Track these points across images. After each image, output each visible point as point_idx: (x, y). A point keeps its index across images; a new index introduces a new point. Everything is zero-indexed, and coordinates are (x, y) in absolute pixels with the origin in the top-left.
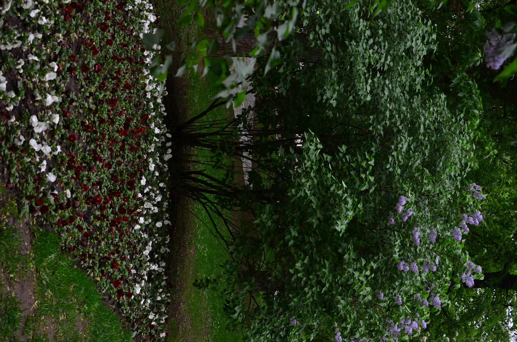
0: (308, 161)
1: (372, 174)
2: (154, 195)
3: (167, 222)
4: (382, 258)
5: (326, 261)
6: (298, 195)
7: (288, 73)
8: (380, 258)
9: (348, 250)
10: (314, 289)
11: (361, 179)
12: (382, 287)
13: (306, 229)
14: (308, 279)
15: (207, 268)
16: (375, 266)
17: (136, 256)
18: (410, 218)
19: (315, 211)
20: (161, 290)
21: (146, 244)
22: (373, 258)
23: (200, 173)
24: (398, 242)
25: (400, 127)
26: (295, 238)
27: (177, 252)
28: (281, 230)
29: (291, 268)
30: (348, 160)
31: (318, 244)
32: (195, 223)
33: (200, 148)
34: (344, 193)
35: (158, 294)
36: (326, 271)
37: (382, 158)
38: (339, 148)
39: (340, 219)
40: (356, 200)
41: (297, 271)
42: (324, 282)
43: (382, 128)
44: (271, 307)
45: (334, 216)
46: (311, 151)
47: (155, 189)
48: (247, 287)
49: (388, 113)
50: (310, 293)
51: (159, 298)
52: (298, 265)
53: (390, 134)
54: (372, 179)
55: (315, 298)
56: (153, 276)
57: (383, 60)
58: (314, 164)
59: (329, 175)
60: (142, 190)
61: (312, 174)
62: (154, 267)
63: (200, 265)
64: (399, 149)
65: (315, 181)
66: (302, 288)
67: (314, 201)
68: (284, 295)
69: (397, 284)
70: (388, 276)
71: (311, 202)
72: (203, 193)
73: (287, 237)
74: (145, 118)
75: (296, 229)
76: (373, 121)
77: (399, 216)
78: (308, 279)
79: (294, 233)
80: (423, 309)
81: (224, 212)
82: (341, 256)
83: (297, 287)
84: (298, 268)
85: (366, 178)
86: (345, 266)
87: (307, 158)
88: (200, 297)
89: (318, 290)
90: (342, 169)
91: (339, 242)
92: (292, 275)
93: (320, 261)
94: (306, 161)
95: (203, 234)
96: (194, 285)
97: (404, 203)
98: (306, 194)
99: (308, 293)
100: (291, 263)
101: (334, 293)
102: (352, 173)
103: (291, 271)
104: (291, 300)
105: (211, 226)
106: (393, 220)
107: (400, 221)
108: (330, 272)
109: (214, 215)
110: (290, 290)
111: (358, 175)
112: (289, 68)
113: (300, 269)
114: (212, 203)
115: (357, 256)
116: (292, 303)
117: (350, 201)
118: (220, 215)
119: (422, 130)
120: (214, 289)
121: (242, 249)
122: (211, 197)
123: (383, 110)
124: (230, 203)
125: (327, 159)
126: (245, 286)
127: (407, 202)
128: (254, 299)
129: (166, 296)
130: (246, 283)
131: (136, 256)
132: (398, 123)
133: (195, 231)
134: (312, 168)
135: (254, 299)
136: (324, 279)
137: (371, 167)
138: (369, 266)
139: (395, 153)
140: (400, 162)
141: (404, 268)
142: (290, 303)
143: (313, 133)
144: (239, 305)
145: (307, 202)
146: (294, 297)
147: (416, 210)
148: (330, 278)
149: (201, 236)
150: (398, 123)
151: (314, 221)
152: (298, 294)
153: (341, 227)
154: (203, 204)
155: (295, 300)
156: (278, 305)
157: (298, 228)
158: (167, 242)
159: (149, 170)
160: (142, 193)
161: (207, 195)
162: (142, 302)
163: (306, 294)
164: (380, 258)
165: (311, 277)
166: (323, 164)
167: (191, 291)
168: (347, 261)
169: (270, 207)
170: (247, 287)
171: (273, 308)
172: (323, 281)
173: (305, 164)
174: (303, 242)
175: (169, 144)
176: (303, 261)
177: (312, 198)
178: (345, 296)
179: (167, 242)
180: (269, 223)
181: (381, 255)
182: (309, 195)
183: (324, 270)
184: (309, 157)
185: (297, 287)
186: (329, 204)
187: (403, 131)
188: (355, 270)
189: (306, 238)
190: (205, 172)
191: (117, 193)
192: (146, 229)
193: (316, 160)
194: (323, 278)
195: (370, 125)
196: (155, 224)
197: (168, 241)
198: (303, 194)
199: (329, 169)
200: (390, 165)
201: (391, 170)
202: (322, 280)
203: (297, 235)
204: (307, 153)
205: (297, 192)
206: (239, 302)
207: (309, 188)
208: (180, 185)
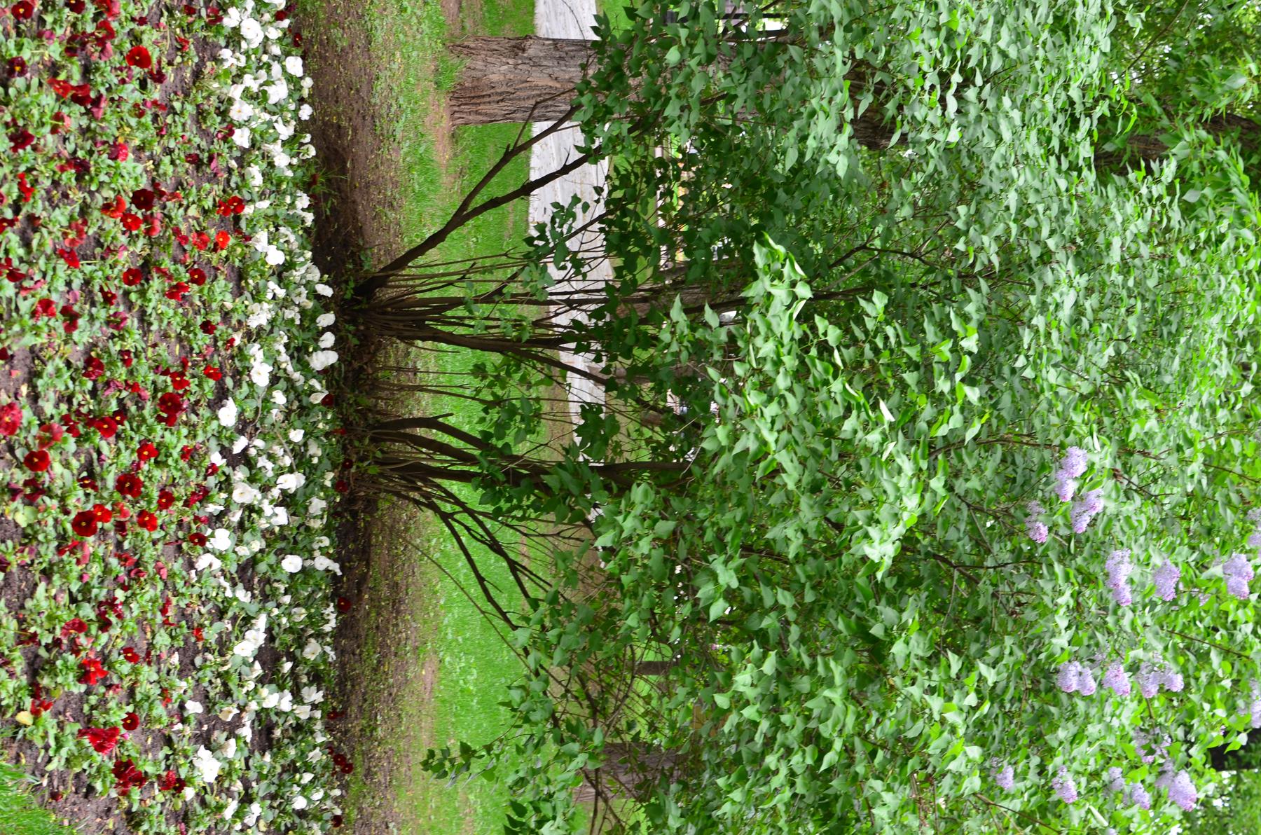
0: (766, 340)
1: (969, 380)
2: (269, 465)
3: (322, 563)
4: (1011, 654)
5: (832, 664)
6: (738, 448)
7: (693, 63)
8: (1007, 651)
9: (903, 628)
10: (796, 759)
11: (938, 400)
12: (1009, 747)
13: (760, 555)
14: (777, 725)
15: (479, 726)
16: (991, 676)
17: (205, 660)
18: (1093, 524)
19: (791, 502)
20: (308, 777)
21: (247, 621)
22: (982, 654)
23: (432, 423)
24: (1065, 599)
25: (1051, 243)
26: (730, 595)
27: (375, 670)
28: (682, 564)
29: (721, 690)
30: (893, 340)
31: (807, 613)
32: (435, 593)
33: (429, 344)
34: (885, 438)
35: (296, 789)
36: (836, 695)
37: (1004, 328)
38: (862, 303)
39: (878, 522)
40: (924, 465)
41: (740, 702)
42: (825, 735)
43: (994, 248)
44: (659, 822)
45: (860, 515)
46: (777, 307)
47: (278, 451)
48: (581, 759)
49: (1012, 199)
50: (784, 771)
51: (300, 803)
52: (743, 680)
53: (1015, 270)
54: (973, 394)
55: (800, 789)
56: (278, 733)
57: (986, 36)
58: (784, 351)
59: (837, 386)
60: (226, 444)
61: (782, 382)
62: (274, 699)
63: (455, 715)
64: (1052, 308)
65: (793, 403)
66: (758, 759)
67: (787, 465)
68: (699, 784)
69: (1062, 734)
70: (1032, 711)
71: (779, 470)
72: (408, 431)
73: (705, 591)
74: (231, 207)
75: (732, 565)
76: (968, 224)
77: (1064, 516)
78: (777, 725)
79: (728, 578)
80: (1130, 819)
81: (505, 536)
82: (877, 650)
83: (739, 754)
84: (741, 689)
85: (953, 391)
86: (897, 681)
87: (762, 329)
88: (456, 810)
89: (809, 761)
90: (874, 367)
91: (872, 604)
92: (724, 714)
93: (814, 666)
94: (759, 341)
95: (461, 624)
96: (426, 765)
97: (1081, 468)
98: (765, 443)
99: (776, 772)
100: (719, 675)
101: (860, 769)
102: (910, 378)
103: (722, 701)
104: (720, 795)
105: (476, 590)
106: (1044, 530)
107: (1064, 531)
108: (850, 696)
109: (480, 553)
110: (719, 765)
111: (927, 384)
112: (696, 51)
113: (751, 693)
114: (471, 513)
115: (930, 647)
116: (727, 808)
117: (908, 467)
118: (496, 547)
119: (1115, 256)
120: (489, 774)
121: (560, 636)
122: (466, 492)
123: (997, 187)
124: (520, 501)
125: (825, 334)
126: (573, 756)
127: (1091, 466)
128: (606, 801)
129: (326, 796)
130: (575, 747)
131: (205, 660)
132: (1045, 232)
133: (436, 615)
134: (778, 363)
135: (606, 801)
136: (830, 723)
137: (967, 360)
138: (974, 676)
139: (1039, 321)
140: (1054, 352)
141: (1082, 684)
142: (718, 808)
143: (781, 249)
144: (554, 818)
145: (766, 468)
146: (732, 787)
147: (1114, 495)
148: (850, 721)
149: (457, 632)
150: (1045, 232)
151: (790, 532)
152: (743, 778)
153: (881, 548)
154: (446, 517)
155: (737, 795)
156: (682, 816)
157: (738, 561)
158: (327, 628)
159: (251, 385)
160: (225, 452)
161: (454, 487)
162: (228, 813)
163: (770, 773)
164: (1007, 651)
165: (786, 719)
166: (814, 352)
167: (426, 789)
168: (900, 664)
169: (646, 494)
170: (581, 759)
171: (665, 825)
172: (826, 730)
173: (757, 350)
174: (754, 606)
175: (327, 319)
176: (759, 666)
177: (783, 458)
178: (895, 779)
179: (327, 628)
180: (645, 546)
181: (1008, 641)
182: (773, 446)
183: (827, 693)
184: (769, 327)
185: (739, 754)
186: (837, 473)
187: (1060, 256)
188: (932, 691)
189: (765, 591)
190: (451, 421)
191: (104, 421)
192: (245, 572)
193: (792, 339)
194: (822, 720)
195: (957, 234)
196: (279, 562)
197: (333, 623)
198: (753, 445)
199: (835, 366)
200: (1027, 357)
201: (1029, 373)
202: (822, 727)
203: (735, 584)
204: (763, 315)
205: (735, 437)
206: (554, 808)
207: (773, 422)
208: (372, 464)
